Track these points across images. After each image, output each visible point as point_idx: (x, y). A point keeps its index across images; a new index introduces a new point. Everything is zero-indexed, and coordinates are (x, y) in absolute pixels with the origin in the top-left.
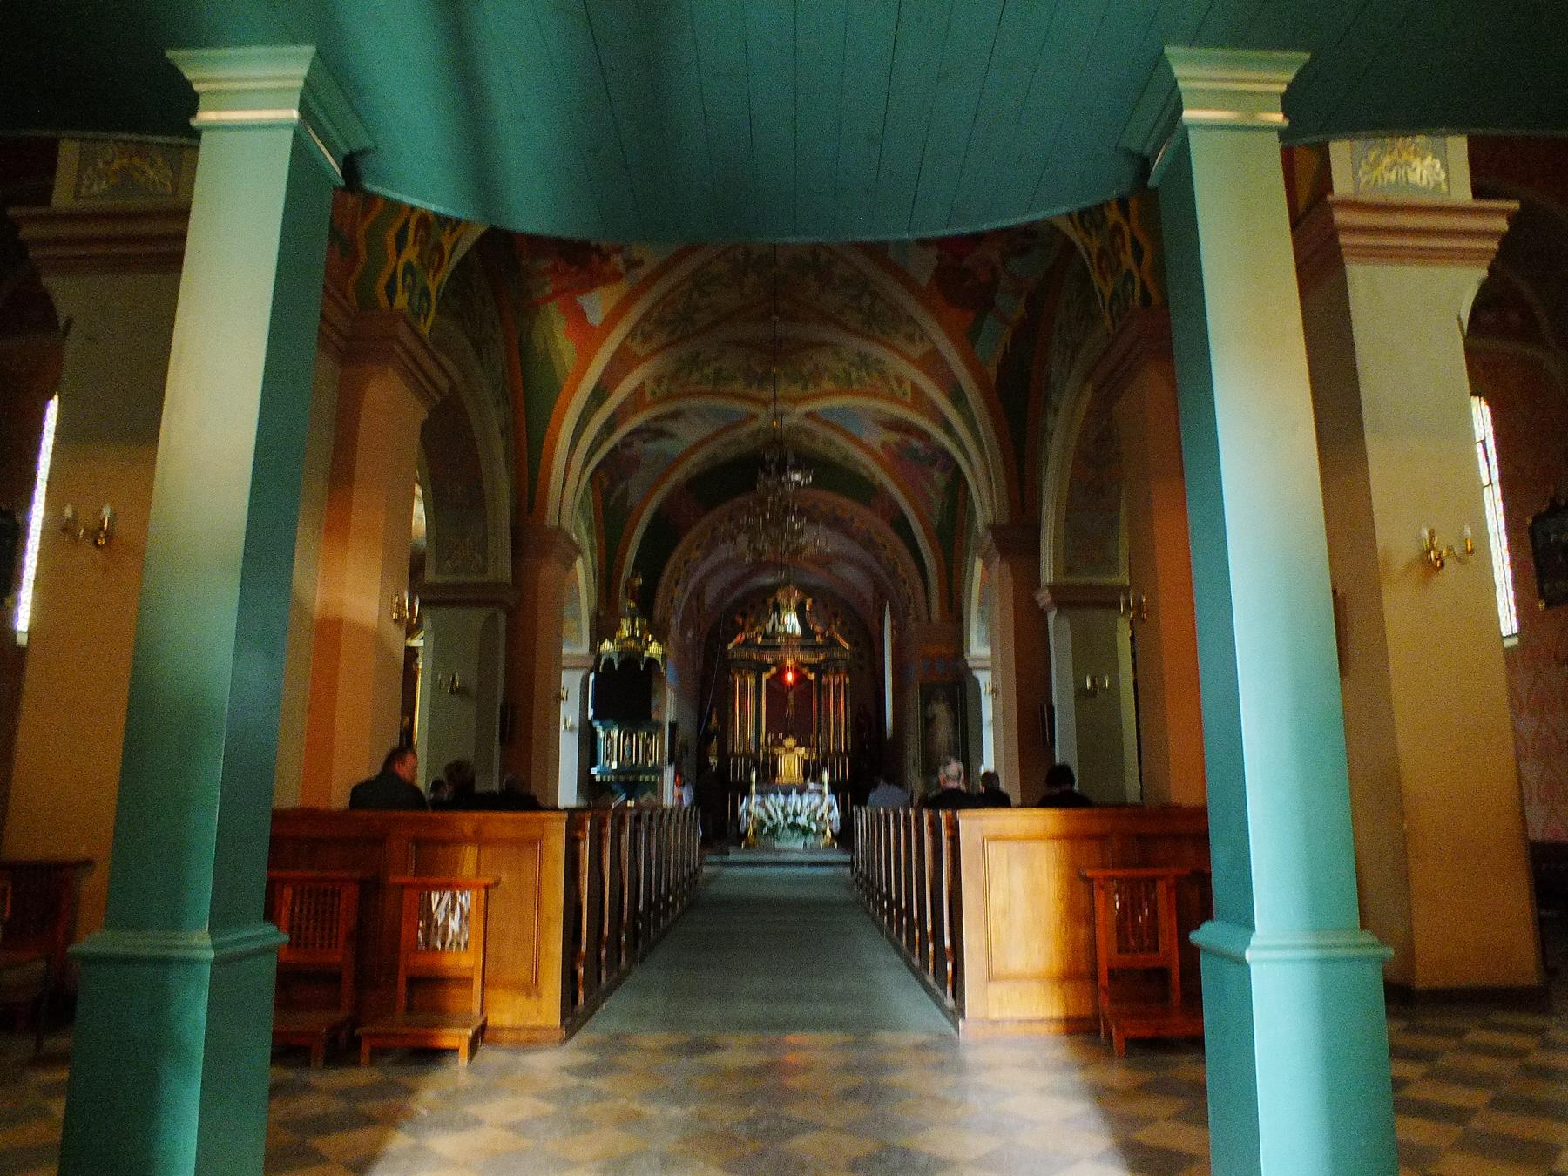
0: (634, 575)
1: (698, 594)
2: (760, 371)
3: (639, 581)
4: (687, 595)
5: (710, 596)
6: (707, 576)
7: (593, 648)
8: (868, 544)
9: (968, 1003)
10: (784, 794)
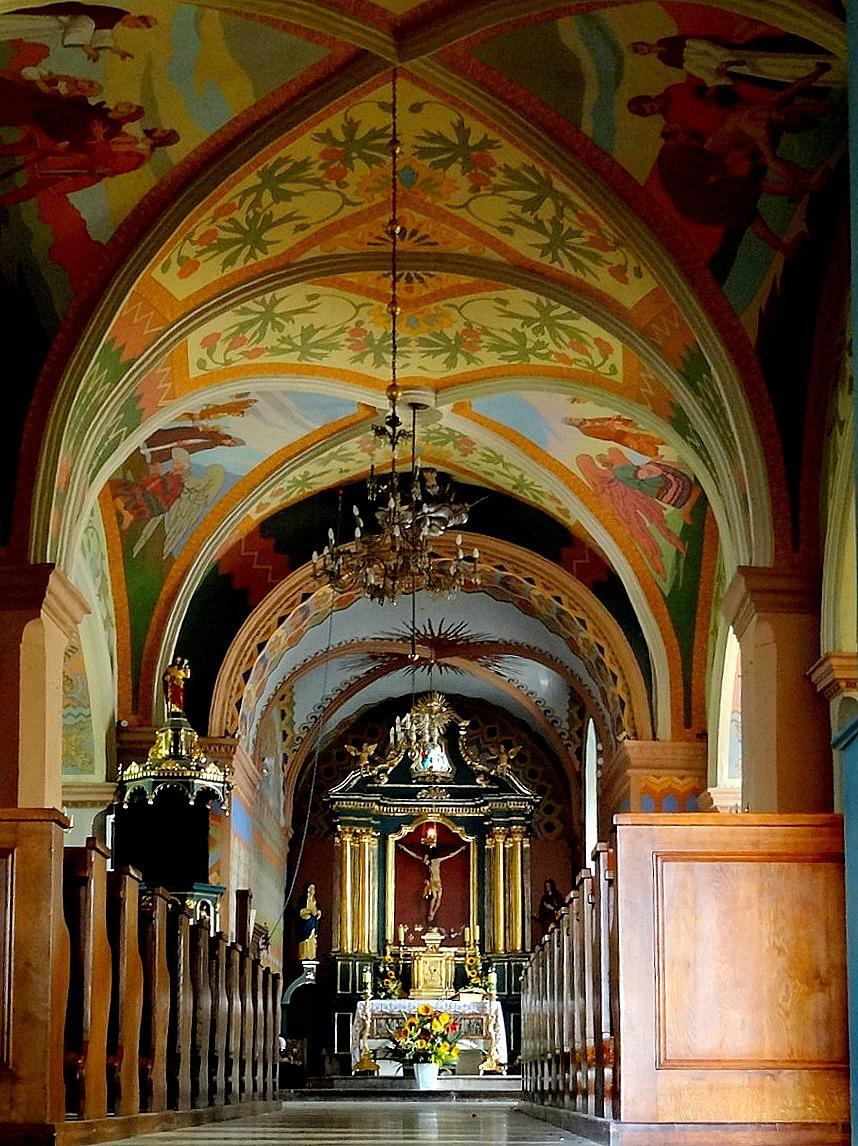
1: (284, 697)
2: (378, 335)
3: (183, 674)
4: (263, 701)
7: (111, 776)
8: (557, 623)
9: (633, 597)
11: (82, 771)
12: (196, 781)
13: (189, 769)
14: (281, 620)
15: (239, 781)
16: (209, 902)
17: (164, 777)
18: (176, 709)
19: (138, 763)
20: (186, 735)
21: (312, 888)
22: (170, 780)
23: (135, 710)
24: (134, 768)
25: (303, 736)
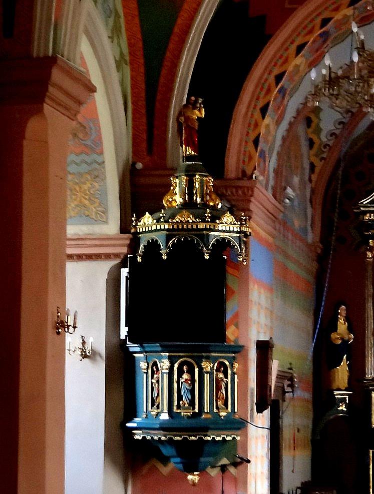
0: (191, 104)
3: (200, 113)
7: (125, 228)
10: (245, 177)
11: (96, 221)
12: (212, 233)
13: (204, 221)
14: (300, 49)
15: (259, 225)
16: (227, 363)
17: (178, 230)
18: (190, 151)
19: (151, 214)
20: (202, 181)
21: (342, 310)
22: (185, 233)
23: (150, 151)
24: (147, 220)
25: (331, 143)
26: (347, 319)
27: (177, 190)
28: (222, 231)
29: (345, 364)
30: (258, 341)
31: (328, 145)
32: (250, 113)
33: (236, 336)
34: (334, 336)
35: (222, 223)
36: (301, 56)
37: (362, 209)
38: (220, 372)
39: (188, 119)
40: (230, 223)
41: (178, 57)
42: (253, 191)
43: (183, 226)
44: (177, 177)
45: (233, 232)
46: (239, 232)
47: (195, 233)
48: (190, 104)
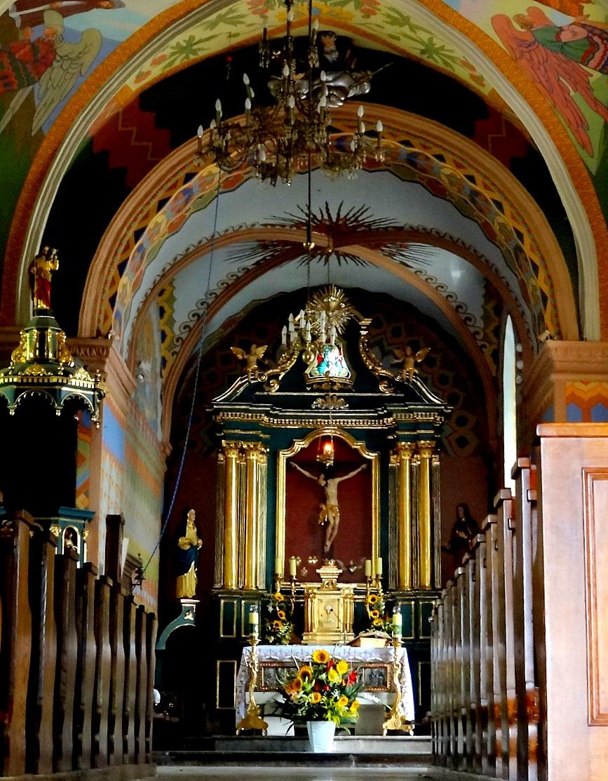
1: (163, 291)
3: (51, 266)
4: (140, 296)
5: (183, 311)
6: (178, 264)
12: (64, 389)
13: (56, 374)
14: (161, 204)
15: (111, 388)
16: (76, 529)
17: (28, 384)
18: (42, 305)
20: (54, 336)
21: (192, 514)
25: (184, 336)
26: (196, 523)
27: (27, 346)
28: (75, 387)
29: (193, 572)
30: (108, 515)
31: (181, 338)
32: (107, 270)
33: (86, 505)
34: (181, 540)
35: (75, 378)
36: (163, 214)
37: (215, 407)
38: (68, 539)
39: (40, 270)
40: (85, 379)
41: (30, 207)
42: (108, 352)
43: (33, 380)
44: (27, 332)
45: (87, 389)
46: (94, 390)
47: (47, 387)
48: (44, 255)
